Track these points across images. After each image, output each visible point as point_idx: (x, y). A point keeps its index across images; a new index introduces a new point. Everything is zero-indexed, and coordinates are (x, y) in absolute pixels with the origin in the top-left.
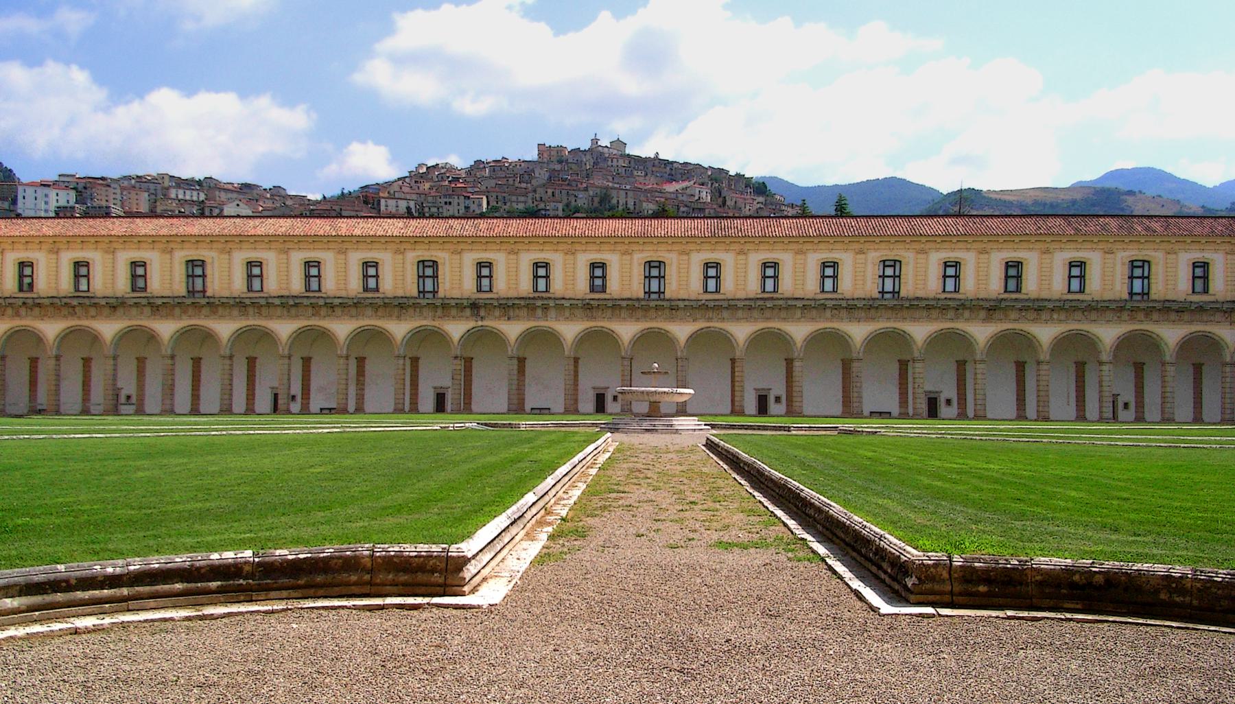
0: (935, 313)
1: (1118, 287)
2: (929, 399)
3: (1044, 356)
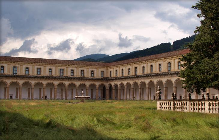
0: (69, 80)
1: (11, 72)
2: (105, 98)
3: (77, 88)
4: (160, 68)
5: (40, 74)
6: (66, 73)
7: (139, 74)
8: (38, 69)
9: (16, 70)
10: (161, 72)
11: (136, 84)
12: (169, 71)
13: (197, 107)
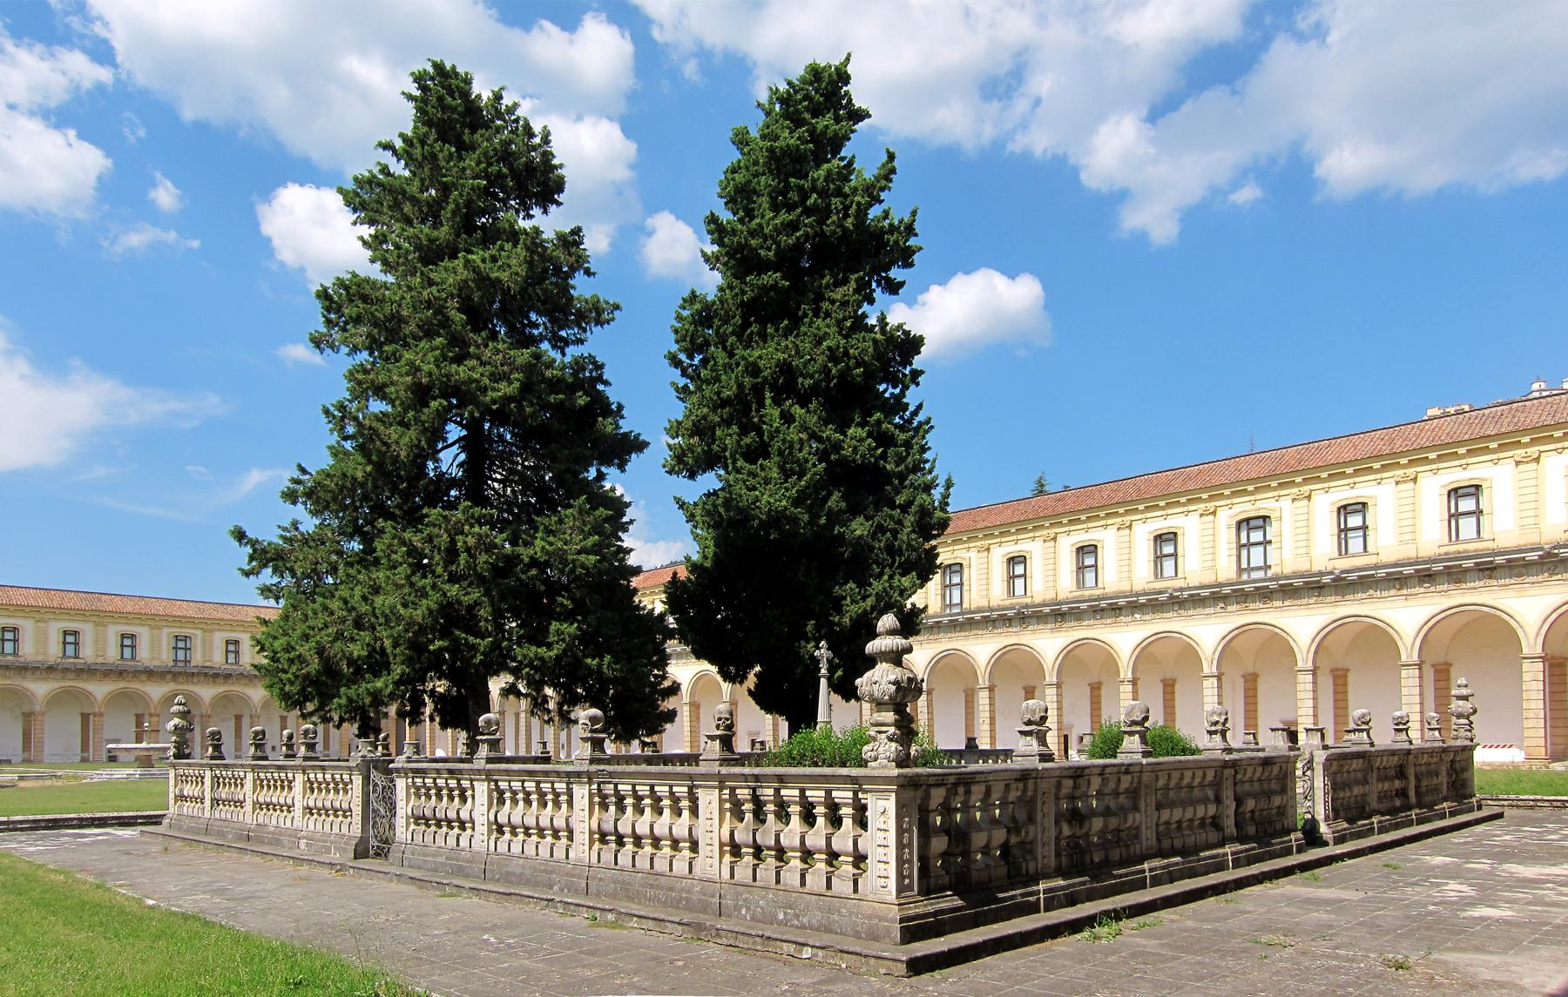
5: (77, 657)
6: (204, 652)
8: (123, 636)
9: (186, 649)
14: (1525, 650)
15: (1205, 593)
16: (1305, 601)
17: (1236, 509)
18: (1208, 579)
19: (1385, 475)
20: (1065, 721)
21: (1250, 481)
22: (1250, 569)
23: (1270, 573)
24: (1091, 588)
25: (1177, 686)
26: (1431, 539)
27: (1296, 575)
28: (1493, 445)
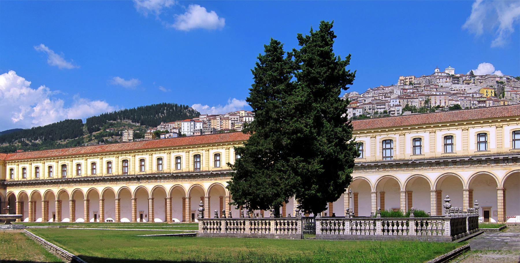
4: (24, 173)
7: (70, 177)
10: (145, 173)
11: (63, 193)
12: (124, 173)
13: (260, 227)
14: (464, 188)
15: (373, 164)
16: (403, 169)
17: (382, 137)
18: (373, 160)
19: (427, 130)
20: (192, 208)
21: (387, 128)
22: (386, 157)
23: (392, 159)
24: (449, 153)
25: (442, 193)
26: (439, 151)
27: (400, 160)
28: (456, 124)
